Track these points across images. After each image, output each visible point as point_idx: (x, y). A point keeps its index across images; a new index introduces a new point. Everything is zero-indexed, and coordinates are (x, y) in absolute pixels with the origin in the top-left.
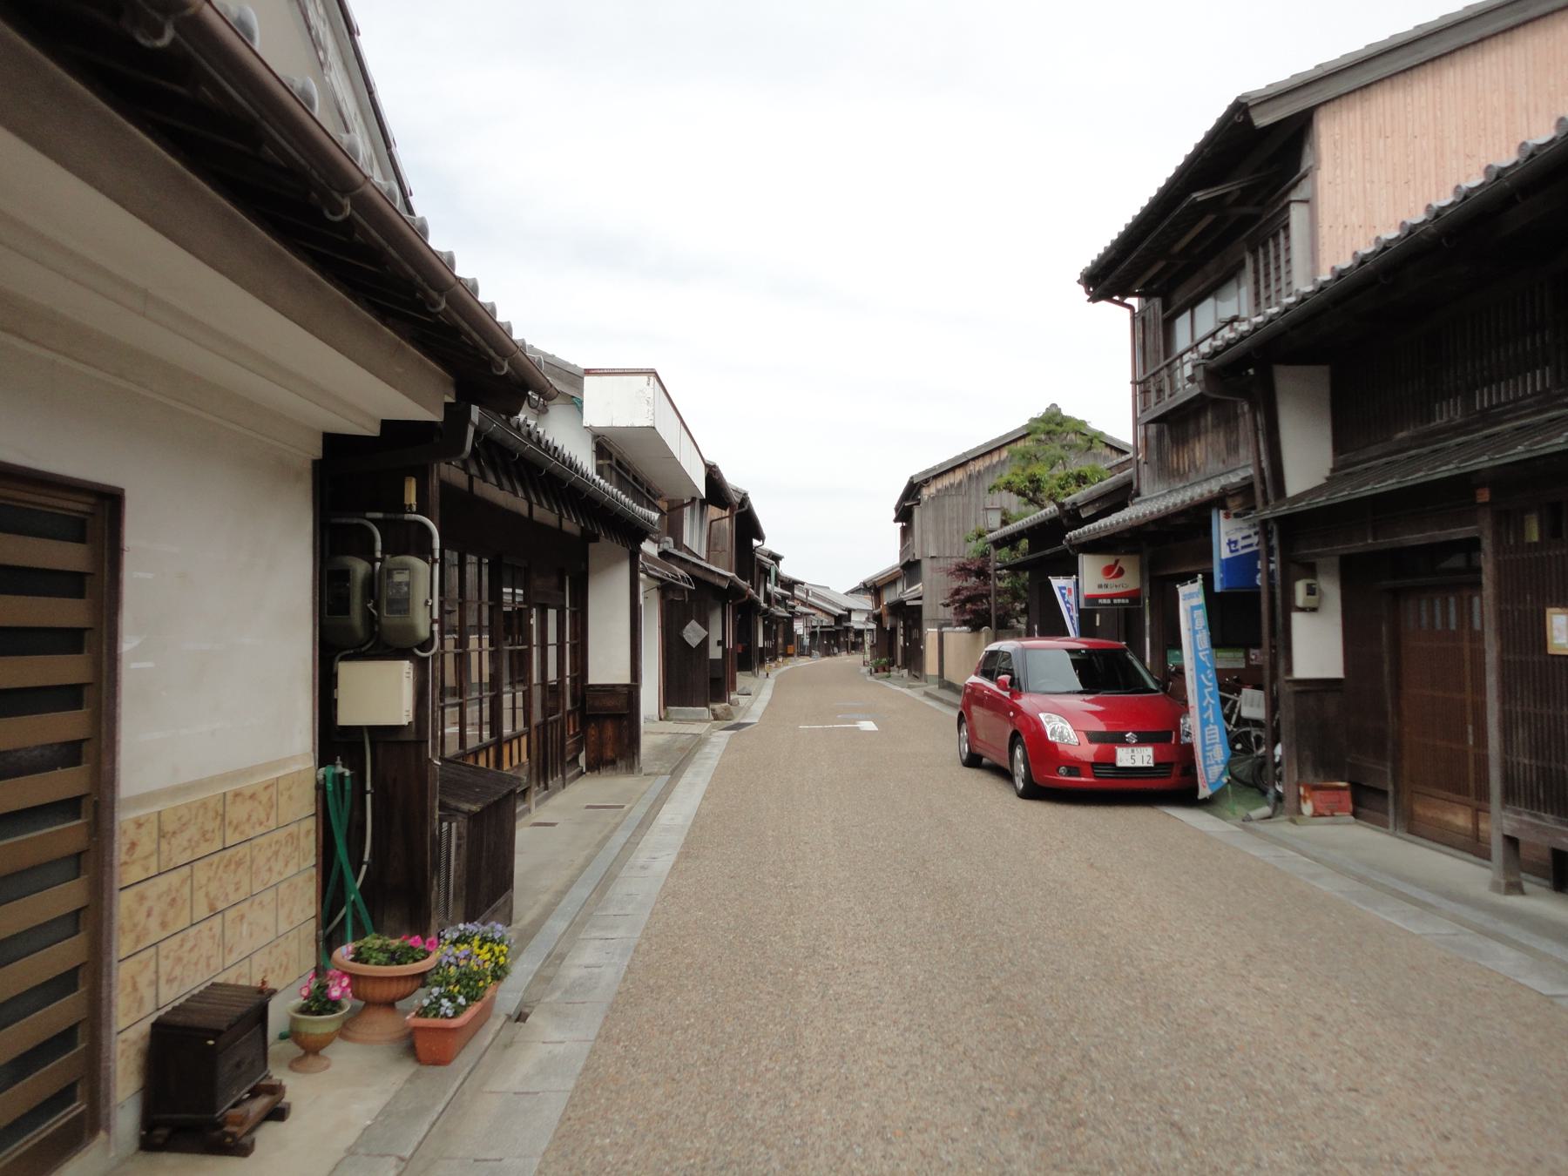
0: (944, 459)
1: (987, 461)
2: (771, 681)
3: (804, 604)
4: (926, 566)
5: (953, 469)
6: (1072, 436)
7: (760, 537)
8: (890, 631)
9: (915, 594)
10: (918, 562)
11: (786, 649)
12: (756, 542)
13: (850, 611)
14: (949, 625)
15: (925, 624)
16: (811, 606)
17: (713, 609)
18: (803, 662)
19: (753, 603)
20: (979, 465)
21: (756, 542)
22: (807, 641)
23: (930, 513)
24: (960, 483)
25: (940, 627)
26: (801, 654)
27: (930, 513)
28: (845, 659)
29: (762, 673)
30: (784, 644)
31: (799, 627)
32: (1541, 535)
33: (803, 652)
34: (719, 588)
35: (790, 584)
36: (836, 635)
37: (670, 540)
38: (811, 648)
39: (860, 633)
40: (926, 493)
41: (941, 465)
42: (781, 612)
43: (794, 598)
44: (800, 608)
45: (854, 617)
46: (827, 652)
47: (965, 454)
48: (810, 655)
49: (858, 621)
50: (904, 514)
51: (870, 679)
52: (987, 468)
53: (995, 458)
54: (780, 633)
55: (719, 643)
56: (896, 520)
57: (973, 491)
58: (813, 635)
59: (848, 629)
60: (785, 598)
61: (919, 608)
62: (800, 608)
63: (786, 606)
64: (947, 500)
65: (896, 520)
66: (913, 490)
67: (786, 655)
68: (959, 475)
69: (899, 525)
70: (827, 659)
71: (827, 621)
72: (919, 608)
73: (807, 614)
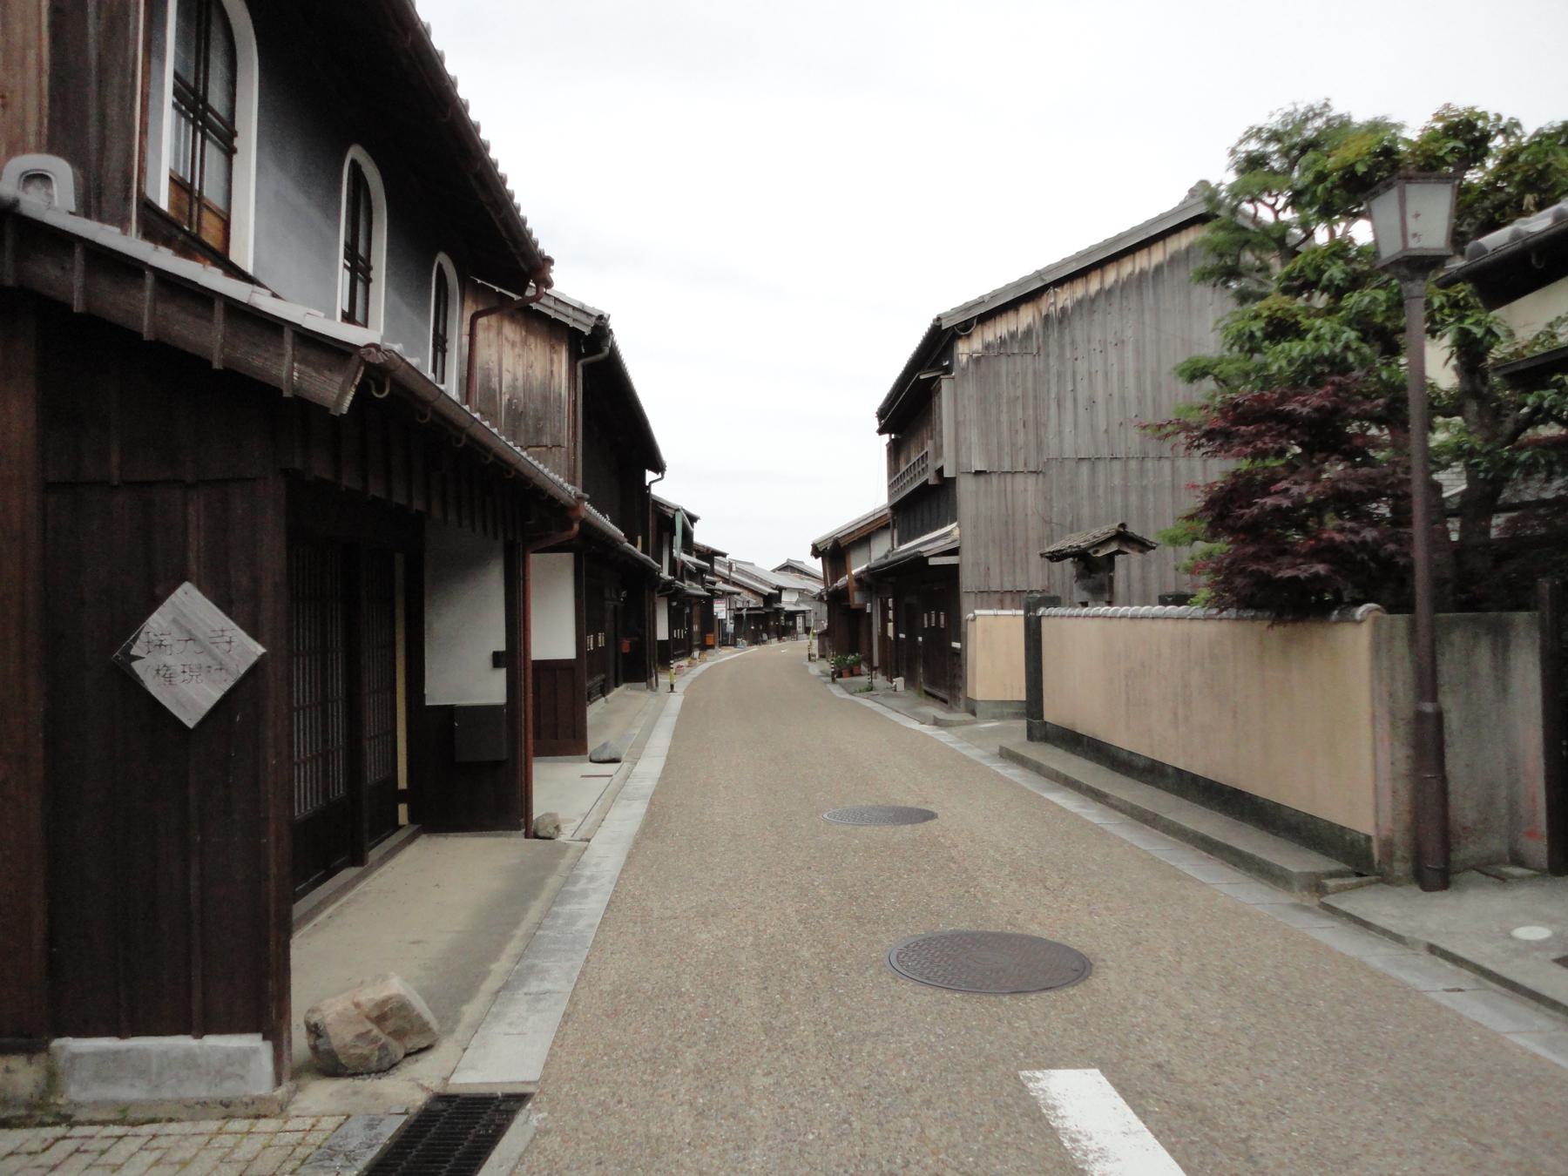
0: (999, 284)
1: (1078, 290)
2: (676, 701)
3: (726, 581)
4: (966, 489)
5: (1013, 305)
6: (1320, 188)
7: (659, 467)
8: (890, 611)
9: (942, 545)
10: (951, 482)
11: (703, 640)
12: (650, 476)
13: (780, 589)
14: (1054, 601)
15: (966, 602)
16: (735, 584)
17: (464, 566)
18: (725, 655)
19: (650, 574)
20: (1063, 298)
21: (650, 476)
22: (730, 627)
23: (970, 389)
24: (1028, 333)
25: (1030, 607)
26: (724, 644)
27: (970, 389)
28: (775, 649)
29: (664, 679)
30: (698, 630)
31: (721, 610)
32: (586, 623)
33: (727, 641)
34: (305, 409)
35: (710, 555)
36: (766, 619)
37: (62, 172)
38: (737, 634)
39: (792, 616)
40: (964, 350)
41: (994, 295)
42: (695, 589)
43: (713, 573)
44: (721, 586)
45: (785, 597)
46: (755, 640)
47: (1039, 274)
48: (735, 644)
49: (788, 602)
50: (908, 412)
51: (836, 691)
52: (1079, 303)
53: (1094, 284)
54: (696, 620)
55: (497, 660)
56: (881, 432)
57: (1053, 347)
58: (738, 619)
59: (779, 611)
60: (701, 570)
61: (955, 569)
62: (721, 586)
63: (703, 582)
64: (1004, 365)
65: (881, 432)
66: (939, 344)
67: (704, 647)
68: (1026, 317)
69: (886, 438)
70: (755, 648)
71: (754, 602)
72: (955, 569)
73: (731, 594)
